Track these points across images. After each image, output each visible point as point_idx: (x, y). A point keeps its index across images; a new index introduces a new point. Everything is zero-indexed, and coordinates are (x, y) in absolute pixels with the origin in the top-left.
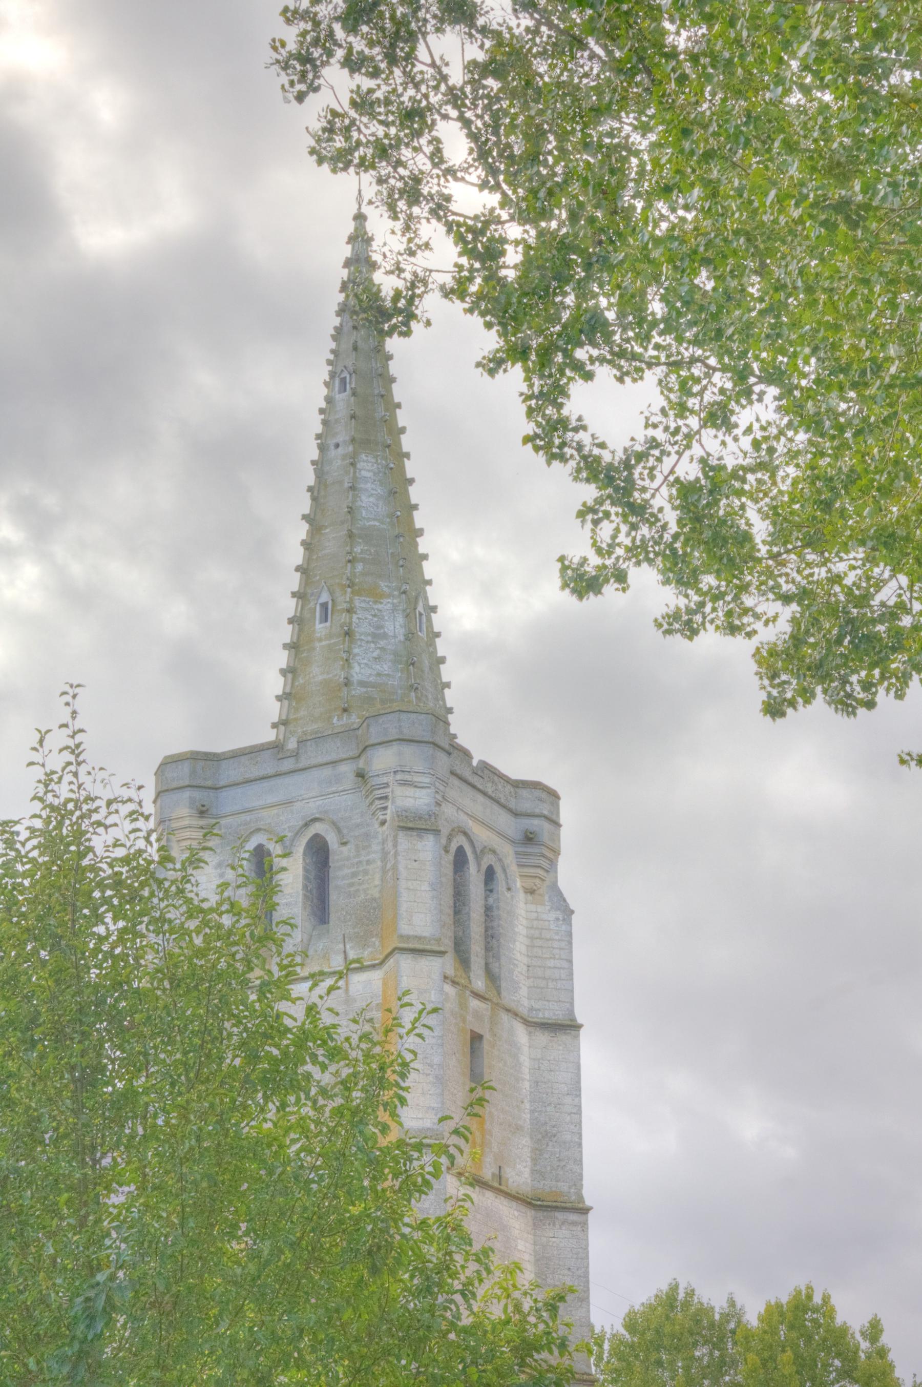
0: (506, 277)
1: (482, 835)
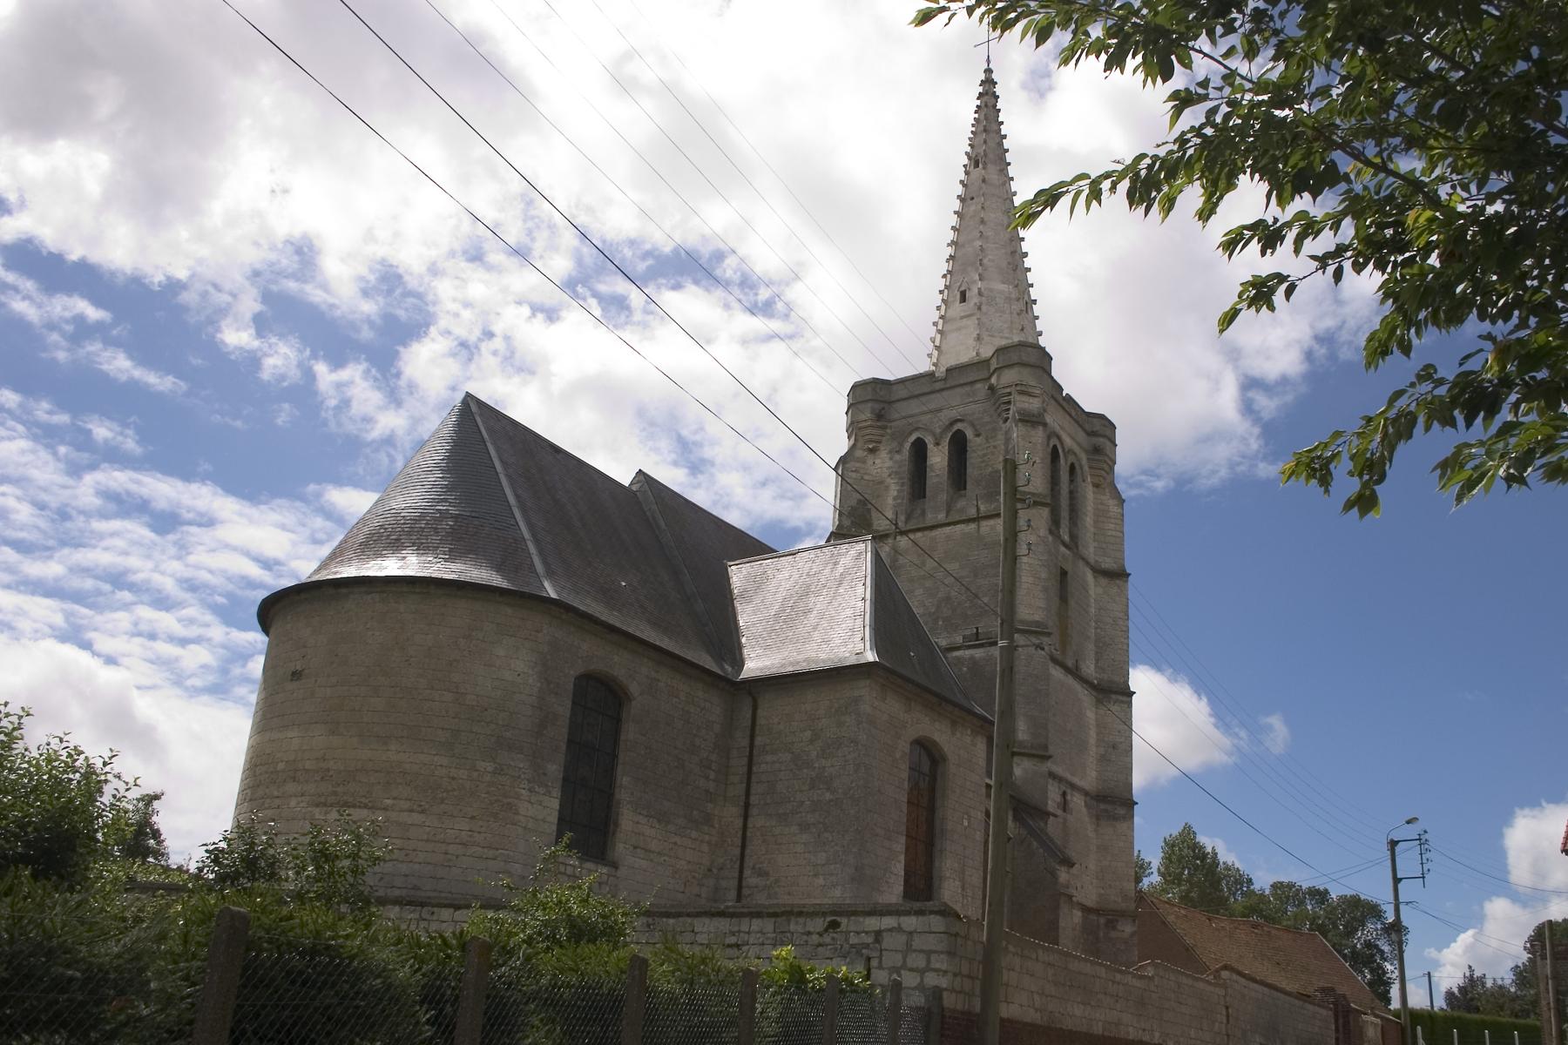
0: (1500, 173)
1: (1068, 441)
